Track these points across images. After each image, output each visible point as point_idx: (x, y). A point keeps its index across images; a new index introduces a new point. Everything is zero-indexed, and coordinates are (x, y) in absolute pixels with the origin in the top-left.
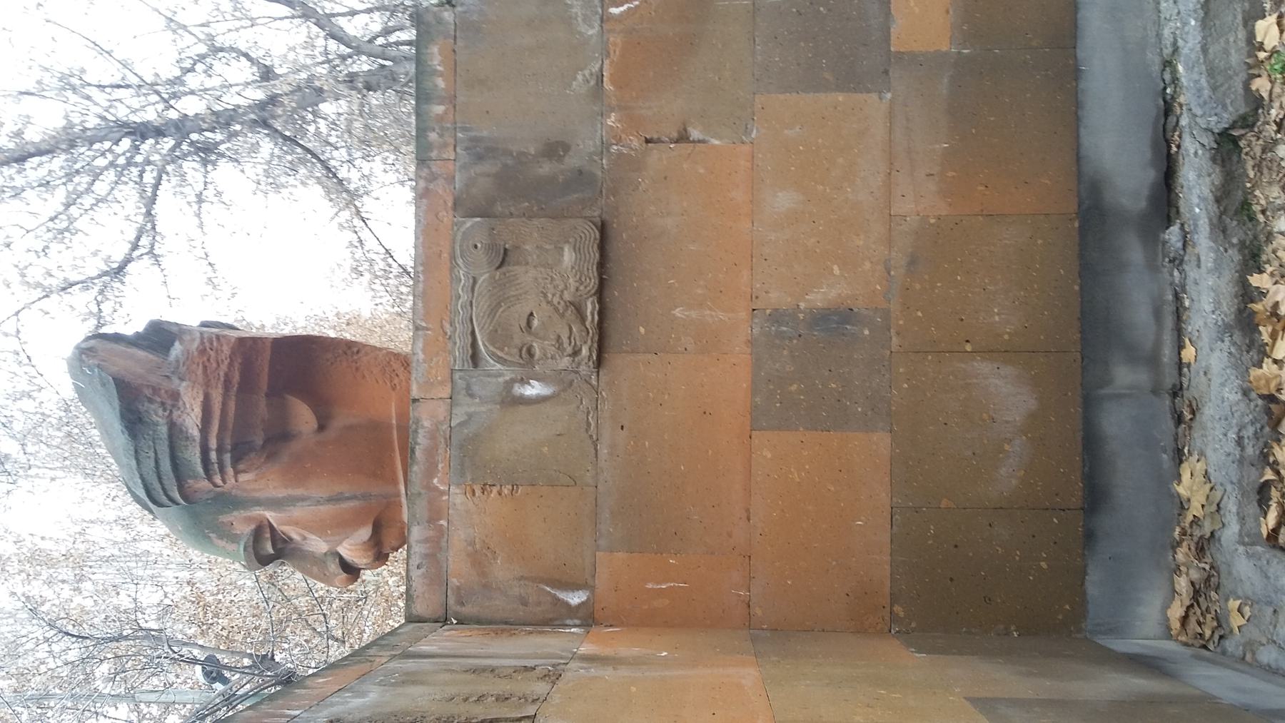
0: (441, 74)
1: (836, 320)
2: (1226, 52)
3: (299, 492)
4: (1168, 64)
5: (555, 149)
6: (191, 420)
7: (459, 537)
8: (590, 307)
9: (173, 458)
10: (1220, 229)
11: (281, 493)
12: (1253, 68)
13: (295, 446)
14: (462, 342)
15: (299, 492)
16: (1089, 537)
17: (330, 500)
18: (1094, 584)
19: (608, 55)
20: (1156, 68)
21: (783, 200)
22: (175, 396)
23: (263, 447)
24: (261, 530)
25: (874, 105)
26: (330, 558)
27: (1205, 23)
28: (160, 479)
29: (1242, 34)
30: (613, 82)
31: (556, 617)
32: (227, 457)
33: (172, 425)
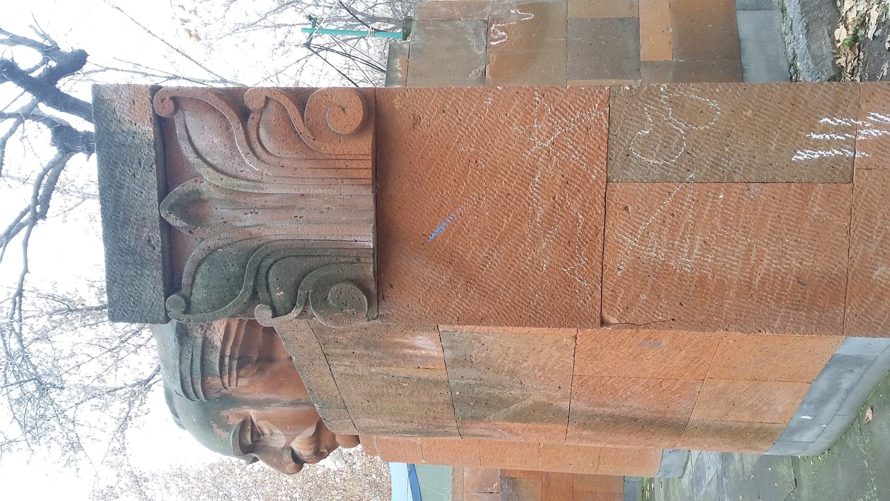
0: (400, 71)
2: (820, 47)
3: (273, 396)
4: (792, 65)
6: (217, 338)
9: (203, 359)
11: (263, 396)
12: (836, 54)
13: (276, 367)
15: (273, 396)
17: (294, 403)
19: (489, 63)
20: (786, 68)
23: (257, 361)
24: (246, 424)
26: (285, 451)
27: (807, 35)
28: (191, 374)
29: (828, 40)
30: (490, 74)
32: (235, 363)
33: (205, 339)
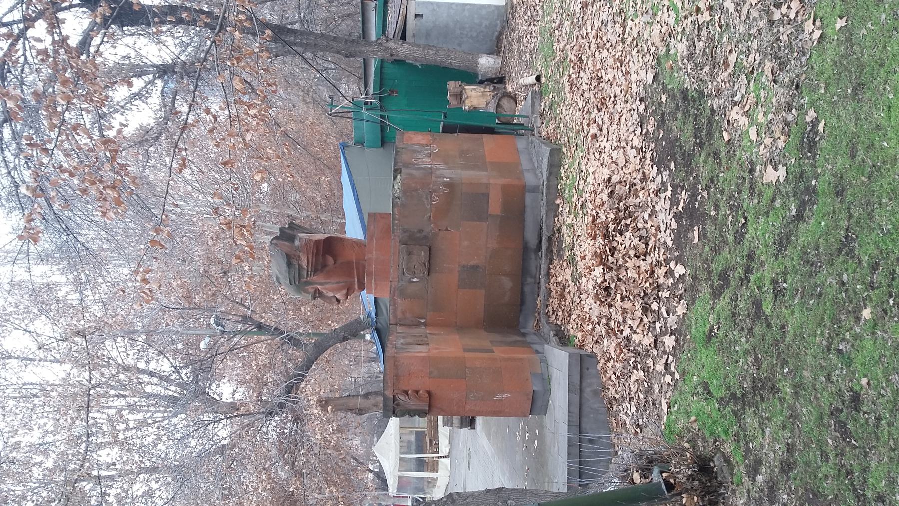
1: (475, 268)
5: (420, 231)
7: (399, 309)
8: (427, 264)
10: (547, 255)
13: (327, 268)
14: (400, 270)
16: (521, 310)
18: (521, 319)
21: (466, 243)
22: (299, 257)
25: (485, 225)
31: (418, 325)
33: (299, 265)
